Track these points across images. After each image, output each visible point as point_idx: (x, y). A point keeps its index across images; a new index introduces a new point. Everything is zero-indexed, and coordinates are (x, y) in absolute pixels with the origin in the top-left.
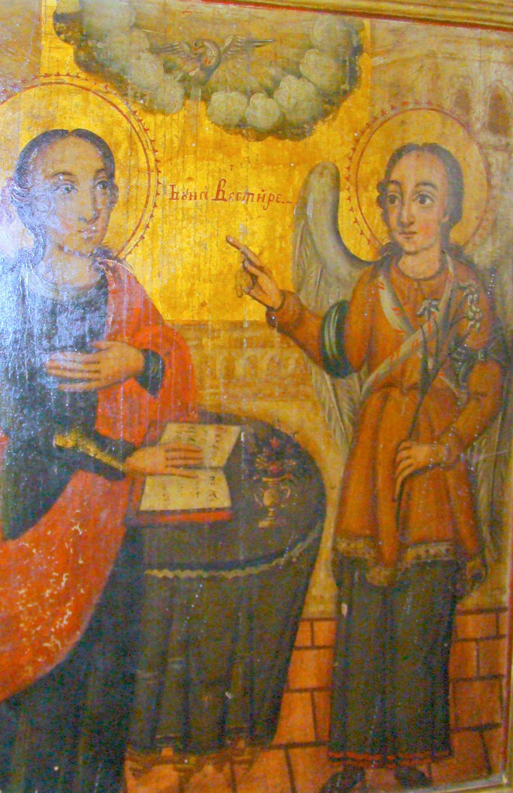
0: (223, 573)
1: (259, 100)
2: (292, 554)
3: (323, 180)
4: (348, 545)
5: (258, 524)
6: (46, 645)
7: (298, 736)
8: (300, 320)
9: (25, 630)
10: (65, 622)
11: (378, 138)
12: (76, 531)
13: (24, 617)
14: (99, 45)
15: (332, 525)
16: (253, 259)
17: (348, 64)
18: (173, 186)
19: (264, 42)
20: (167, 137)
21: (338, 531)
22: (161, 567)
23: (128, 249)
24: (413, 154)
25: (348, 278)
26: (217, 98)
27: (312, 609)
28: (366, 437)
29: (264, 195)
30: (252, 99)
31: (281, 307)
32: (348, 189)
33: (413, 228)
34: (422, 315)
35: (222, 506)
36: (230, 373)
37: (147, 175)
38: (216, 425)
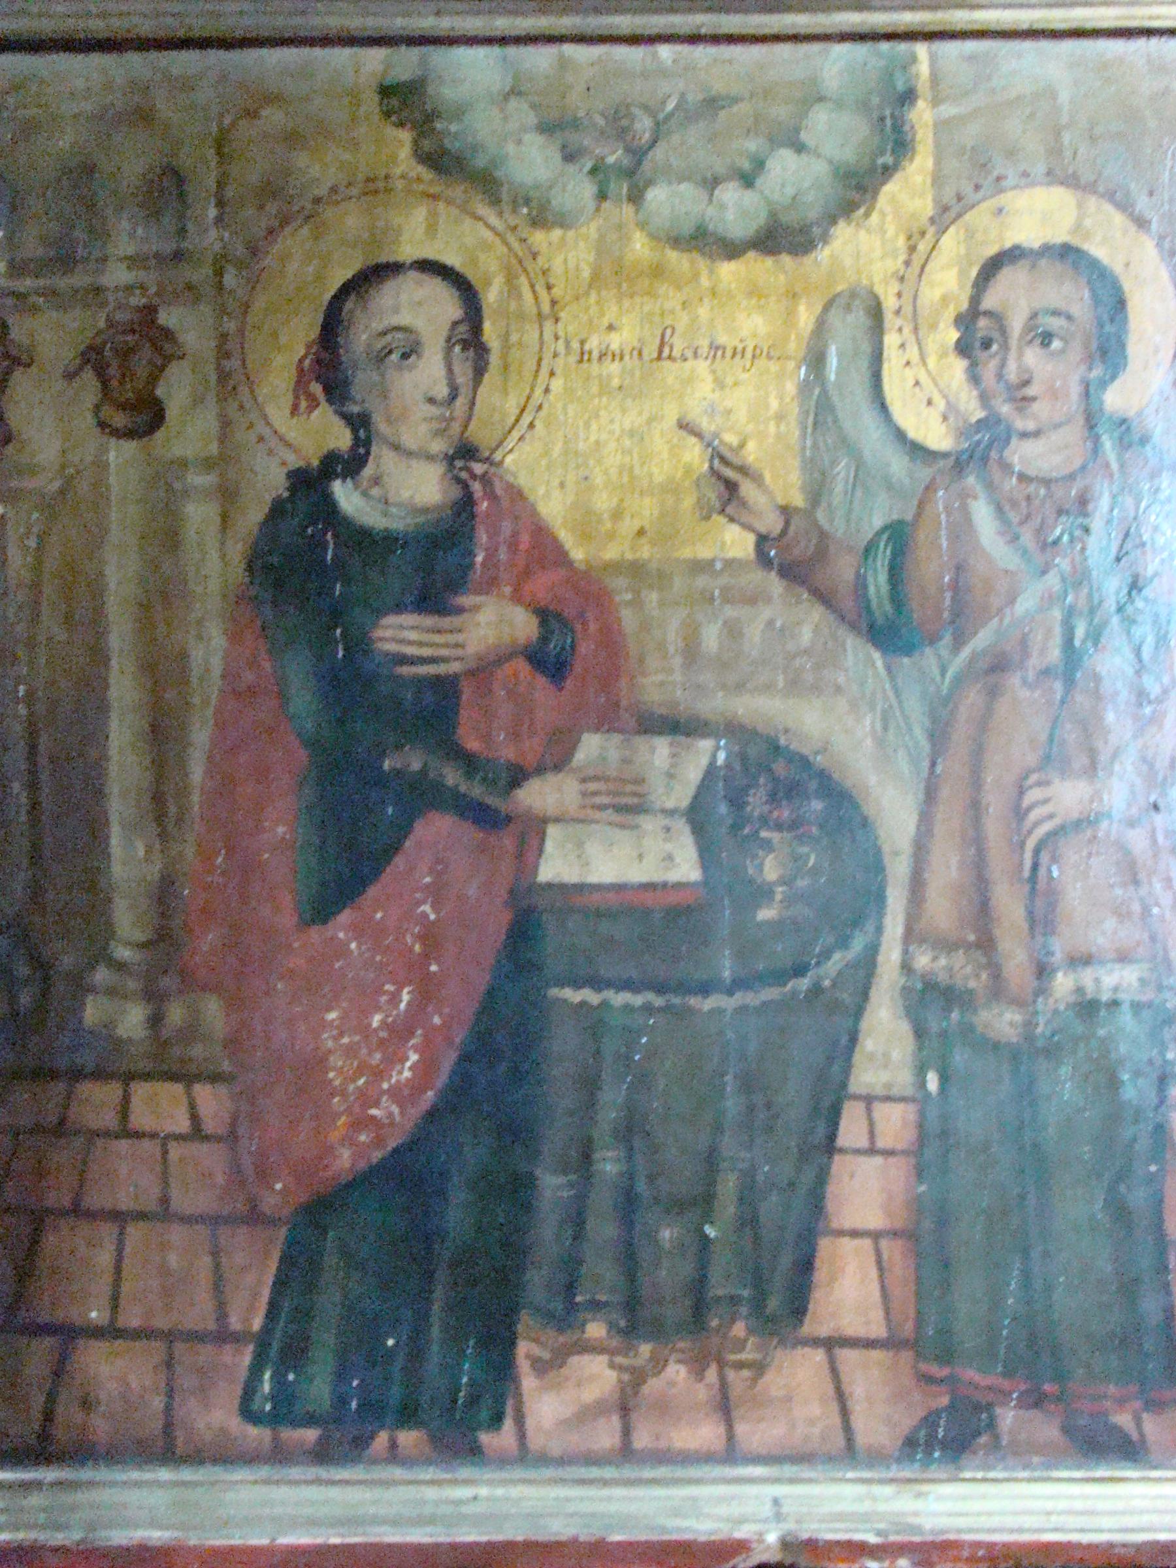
0: (693, 1001)
1: (730, 193)
2: (821, 971)
3: (850, 318)
4: (935, 959)
5: (754, 917)
6: (374, 1112)
7: (853, 1326)
8: (822, 553)
9: (337, 1083)
10: (407, 1074)
11: (951, 241)
12: (425, 915)
13: (336, 1061)
14: (453, 128)
15: (901, 919)
16: (728, 454)
17: (888, 122)
18: (582, 342)
19: (736, 100)
20: (569, 263)
21: (910, 935)
22: (577, 985)
23: (510, 443)
24: (1024, 264)
25: (907, 481)
26: (656, 195)
27: (866, 1076)
28: (953, 766)
29: (744, 349)
30: (716, 192)
31: (784, 532)
32: (900, 330)
33: (1030, 391)
34: (1056, 543)
35: (684, 880)
36: (691, 651)
37: (537, 326)
38: (669, 738)
